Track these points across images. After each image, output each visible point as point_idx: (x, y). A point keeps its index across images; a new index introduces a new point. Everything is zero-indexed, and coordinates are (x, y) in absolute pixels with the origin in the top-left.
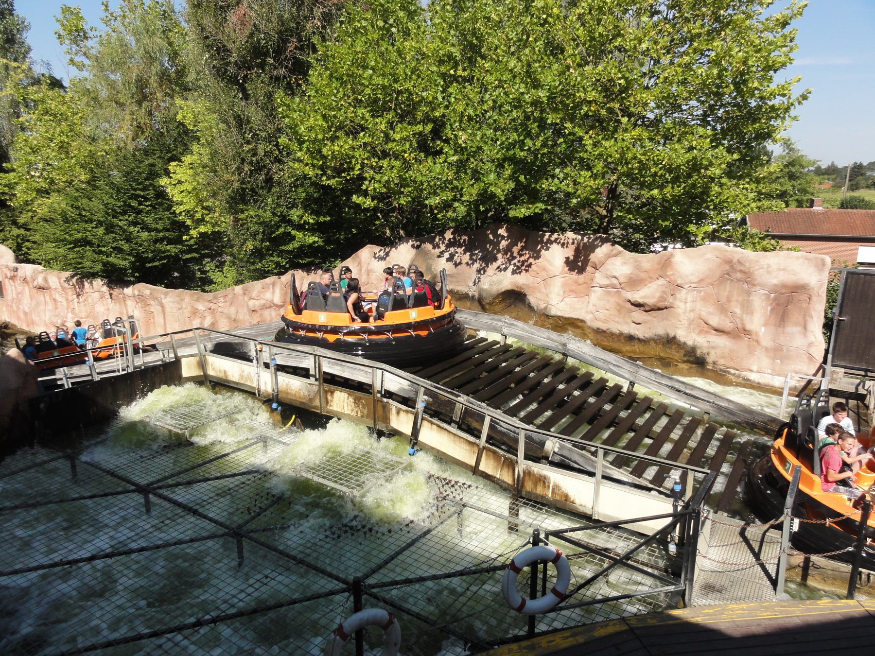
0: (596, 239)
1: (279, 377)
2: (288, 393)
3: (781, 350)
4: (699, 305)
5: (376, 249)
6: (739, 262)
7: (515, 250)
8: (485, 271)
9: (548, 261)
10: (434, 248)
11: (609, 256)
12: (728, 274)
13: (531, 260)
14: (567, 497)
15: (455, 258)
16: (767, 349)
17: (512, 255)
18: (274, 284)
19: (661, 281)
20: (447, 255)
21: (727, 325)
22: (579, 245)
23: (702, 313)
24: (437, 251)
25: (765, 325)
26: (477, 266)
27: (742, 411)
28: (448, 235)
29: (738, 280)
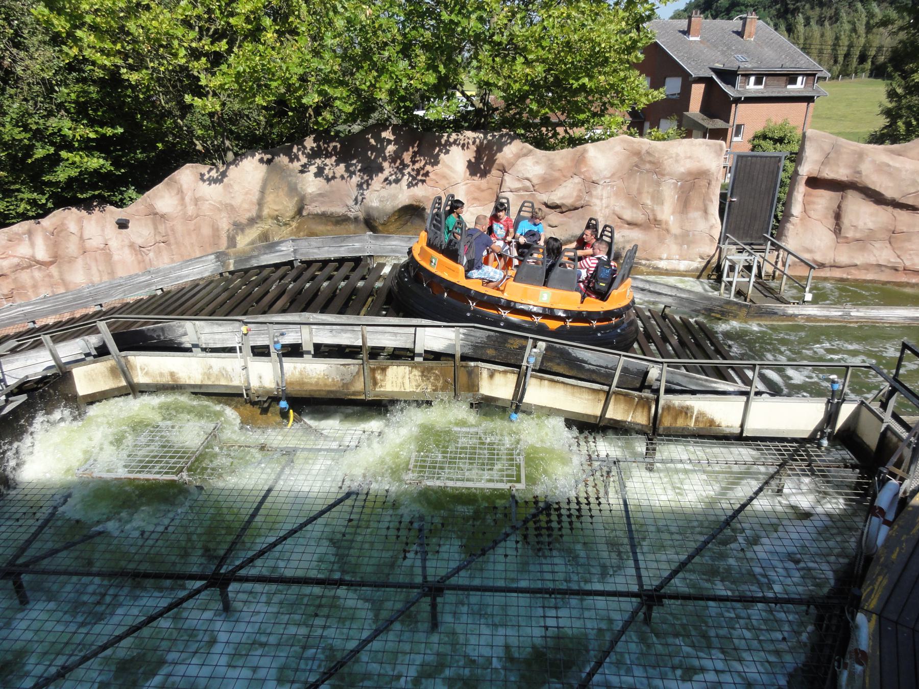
0: (502, 136)
1: (285, 365)
2: (304, 383)
3: (688, 235)
4: (612, 201)
5: (204, 169)
6: (648, 153)
7: (407, 157)
8: (368, 185)
9: (448, 167)
10: (291, 161)
11: (518, 156)
12: (637, 166)
13: (428, 168)
14: (712, 422)
15: (326, 172)
16: (676, 236)
17: (402, 163)
18: (30, 233)
19: (577, 179)
20: (313, 169)
21: (639, 217)
22: (481, 143)
23: (616, 208)
24: (297, 165)
25: (673, 213)
26: (356, 179)
27: (701, 299)
28: (309, 143)
29: (648, 171)
